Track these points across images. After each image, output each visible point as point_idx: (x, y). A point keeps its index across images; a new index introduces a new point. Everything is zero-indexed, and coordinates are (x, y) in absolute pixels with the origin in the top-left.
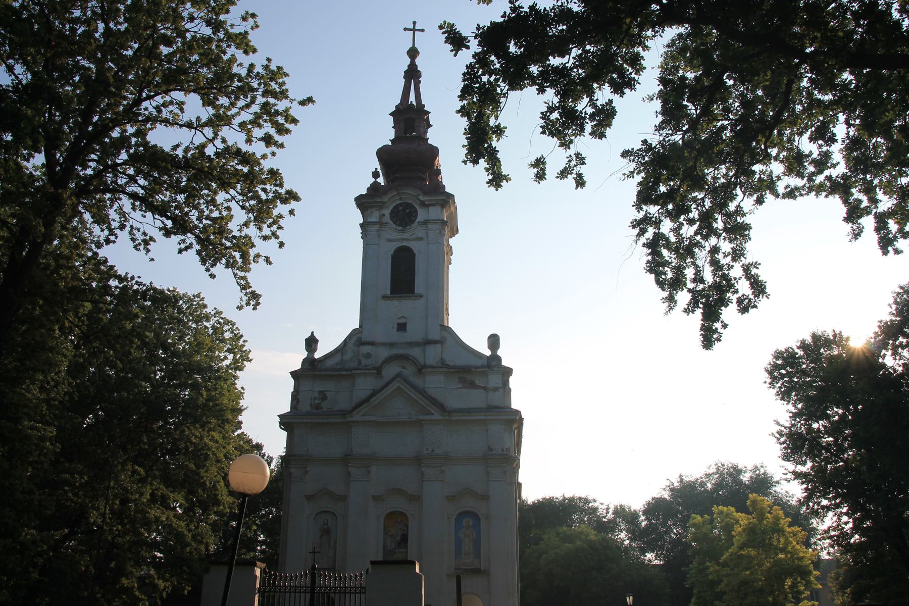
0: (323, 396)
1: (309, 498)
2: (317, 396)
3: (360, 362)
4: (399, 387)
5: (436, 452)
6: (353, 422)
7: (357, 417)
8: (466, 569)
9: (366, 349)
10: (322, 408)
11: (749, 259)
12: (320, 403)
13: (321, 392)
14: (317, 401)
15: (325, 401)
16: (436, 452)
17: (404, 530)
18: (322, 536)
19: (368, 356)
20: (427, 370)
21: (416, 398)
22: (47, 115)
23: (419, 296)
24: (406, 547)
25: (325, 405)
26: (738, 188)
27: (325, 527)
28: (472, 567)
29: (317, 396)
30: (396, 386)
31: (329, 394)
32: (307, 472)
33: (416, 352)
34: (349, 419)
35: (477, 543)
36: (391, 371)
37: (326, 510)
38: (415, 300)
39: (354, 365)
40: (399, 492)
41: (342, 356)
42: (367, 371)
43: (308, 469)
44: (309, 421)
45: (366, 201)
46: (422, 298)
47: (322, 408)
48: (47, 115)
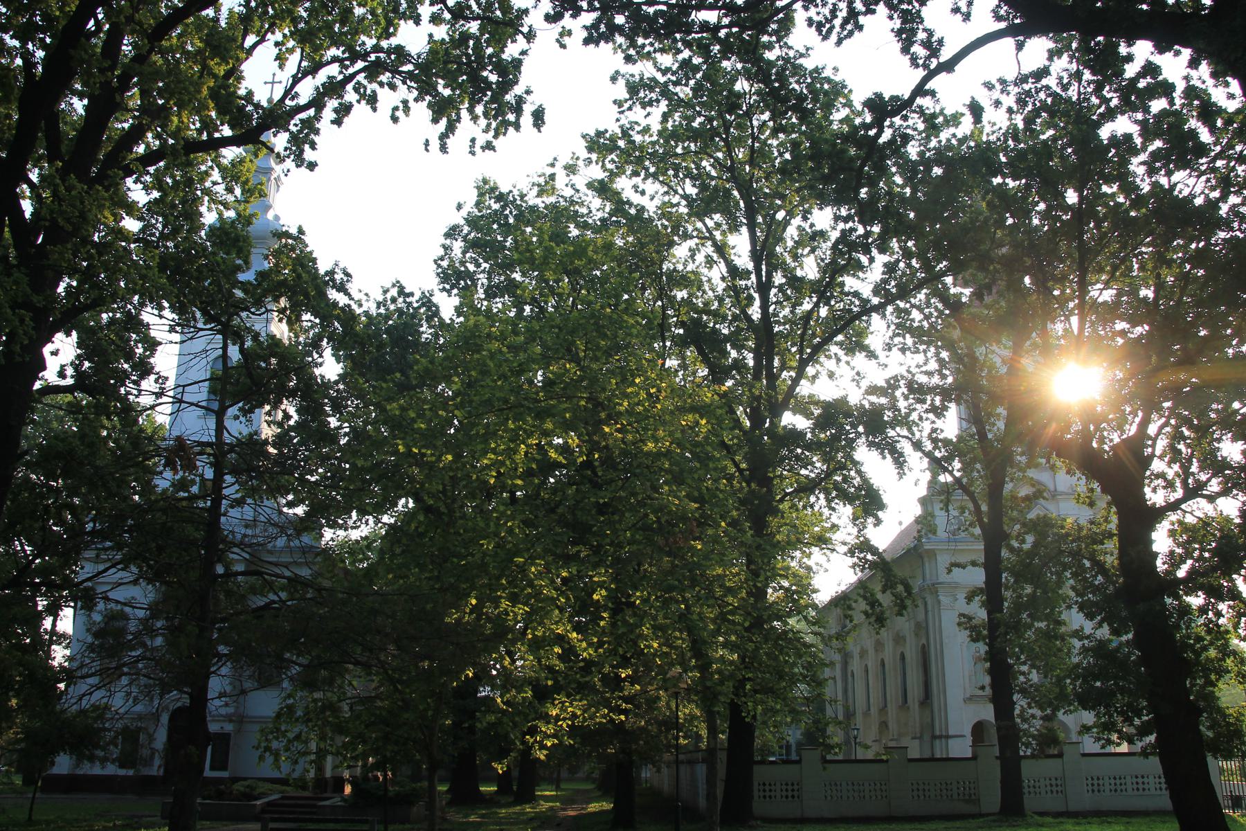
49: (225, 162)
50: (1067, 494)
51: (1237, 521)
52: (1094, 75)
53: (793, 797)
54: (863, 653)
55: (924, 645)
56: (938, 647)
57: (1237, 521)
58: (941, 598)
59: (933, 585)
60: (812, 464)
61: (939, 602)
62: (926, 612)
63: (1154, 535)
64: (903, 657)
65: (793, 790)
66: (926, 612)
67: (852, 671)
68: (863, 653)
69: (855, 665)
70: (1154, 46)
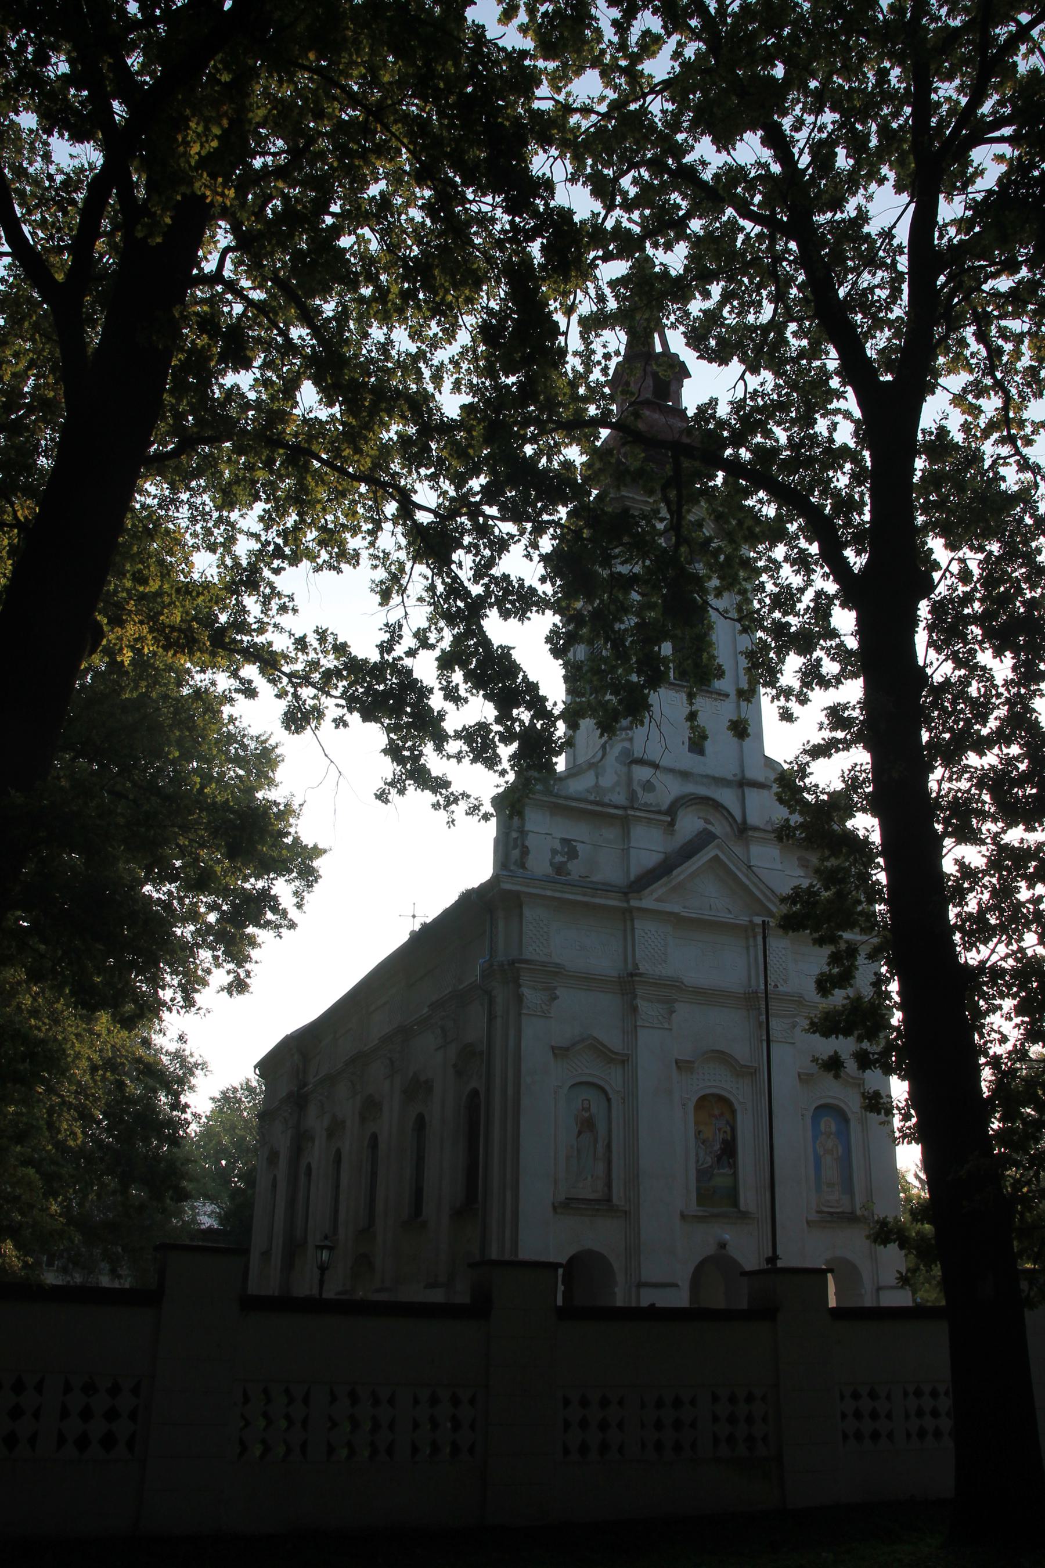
0: (570, 848)
1: (560, 1052)
2: (559, 848)
3: (632, 796)
4: (717, 856)
5: (781, 988)
6: (640, 909)
7: (648, 901)
8: (831, 1214)
9: (642, 773)
10: (569, 874)
11: (382, 548)
12: (565, 863)
13: (565, 841)
14: (559, 859)
15: (575, 861)
16: (781, 988)
17: (725, 1132)
18: (580, 1133)
19: (648, 786)
20: (756, 834)
21: (747, 882)
22: (1002, 589)
23: (720, 694)
24: (734, 1166)
25: (575, 868)
26: (582, 371)
27: (586, 1115)
28: (838, 1210)
29: (559, 848)
30: (712, 854)
31: (580, 847)
32: (555, 998)
33: (727, 797)
34: (634, 903)
35: (846, 1162)
36: (689, 824)
37: (584, 1079)
38: (716, 700)
39: (620, 798)
40: (722, 1057)
41: (597, 778)
42: (652, 816)
43: (557, 992)
44: (557, 895)
45: (631, 495)
46: (728, 700)
47: (569, 874)
48: (1002, 589)
49: (948, 228)
50: (765, 831)
51: (817, 416)
52: (541, 82)
53: (108, 1441)
54: (335, 1128)
55: (475, 1093)
56: (510, 1091)
57: (817, 416)
58: (526, 991)
59: (513, 962)
60: (227, 883)
61: (520, 999)
62: (491, 1018)
63: (875, 821)
64: (421, 1123)
65: (111, 1415)
66: (491, 1018)
67: (309, 1167)
68: (335, 1128)
69: (317, 1155)
70: (139, 8)
